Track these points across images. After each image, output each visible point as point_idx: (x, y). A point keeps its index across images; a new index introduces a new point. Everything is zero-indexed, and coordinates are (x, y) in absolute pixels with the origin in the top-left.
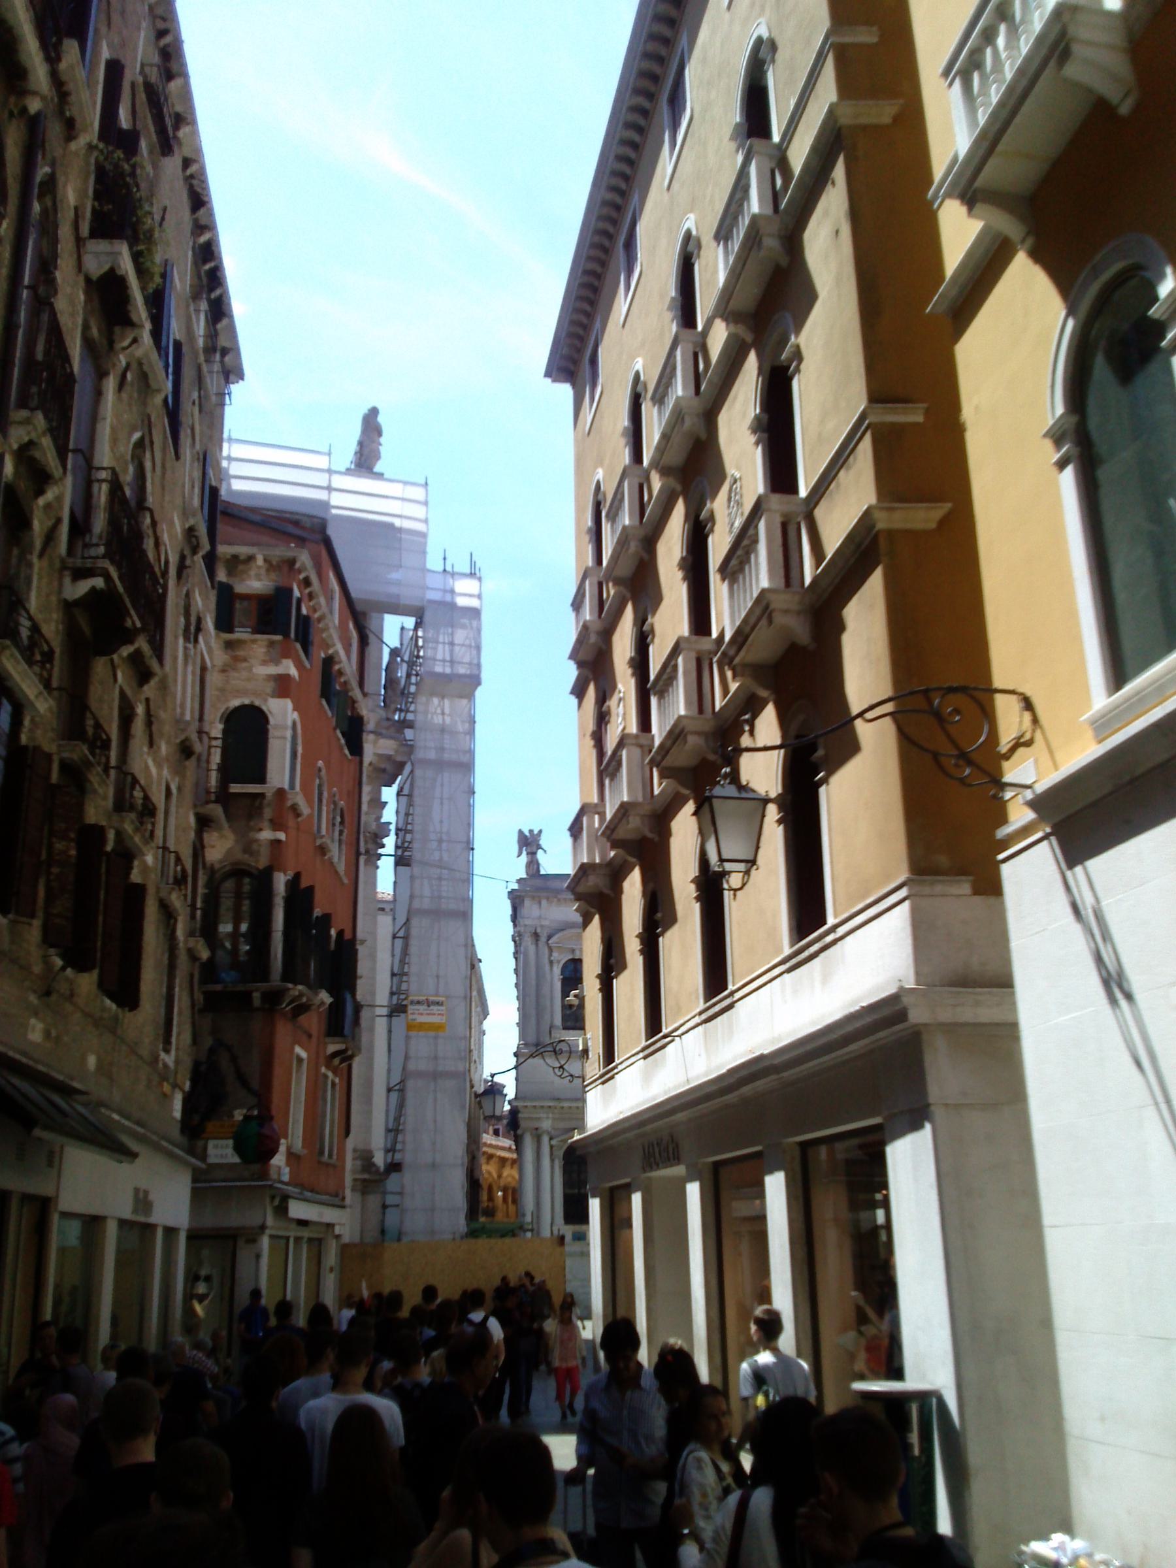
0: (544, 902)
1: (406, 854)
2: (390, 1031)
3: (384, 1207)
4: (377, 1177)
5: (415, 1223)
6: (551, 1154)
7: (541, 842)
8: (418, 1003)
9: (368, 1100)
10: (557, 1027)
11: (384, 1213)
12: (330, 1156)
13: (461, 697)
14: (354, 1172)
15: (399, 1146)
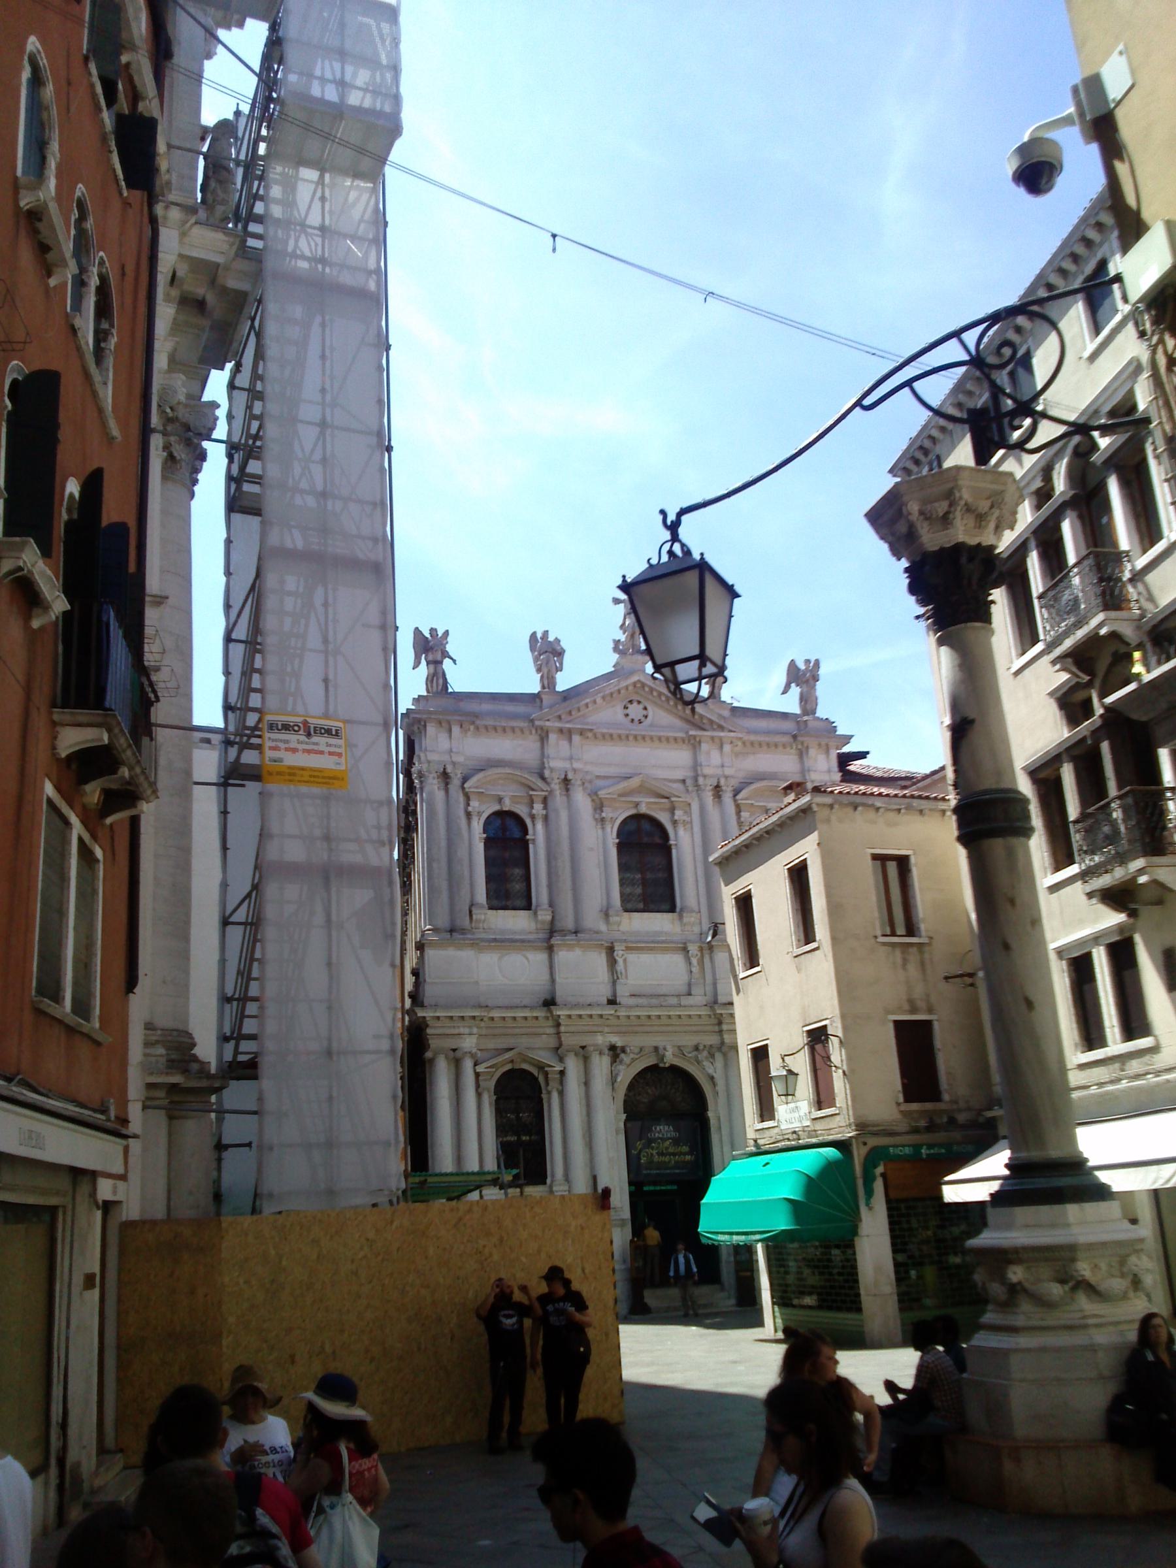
0: (456, 730)
1: (258, 443)
2: (224, 813)
3: (220, 1147)
4: (204, 1083)
5: (291, 1176)
6: (478, 1086)
7: (449, 648)
8: (286, 727)
9: (180, 929)
10: (481, 906)
11: (219, 1160)
12: (81, 1007)
13: (357, 175)
14: (147, 1069)
15: (254, 990)
